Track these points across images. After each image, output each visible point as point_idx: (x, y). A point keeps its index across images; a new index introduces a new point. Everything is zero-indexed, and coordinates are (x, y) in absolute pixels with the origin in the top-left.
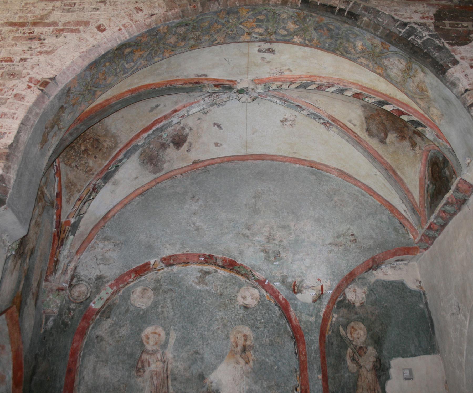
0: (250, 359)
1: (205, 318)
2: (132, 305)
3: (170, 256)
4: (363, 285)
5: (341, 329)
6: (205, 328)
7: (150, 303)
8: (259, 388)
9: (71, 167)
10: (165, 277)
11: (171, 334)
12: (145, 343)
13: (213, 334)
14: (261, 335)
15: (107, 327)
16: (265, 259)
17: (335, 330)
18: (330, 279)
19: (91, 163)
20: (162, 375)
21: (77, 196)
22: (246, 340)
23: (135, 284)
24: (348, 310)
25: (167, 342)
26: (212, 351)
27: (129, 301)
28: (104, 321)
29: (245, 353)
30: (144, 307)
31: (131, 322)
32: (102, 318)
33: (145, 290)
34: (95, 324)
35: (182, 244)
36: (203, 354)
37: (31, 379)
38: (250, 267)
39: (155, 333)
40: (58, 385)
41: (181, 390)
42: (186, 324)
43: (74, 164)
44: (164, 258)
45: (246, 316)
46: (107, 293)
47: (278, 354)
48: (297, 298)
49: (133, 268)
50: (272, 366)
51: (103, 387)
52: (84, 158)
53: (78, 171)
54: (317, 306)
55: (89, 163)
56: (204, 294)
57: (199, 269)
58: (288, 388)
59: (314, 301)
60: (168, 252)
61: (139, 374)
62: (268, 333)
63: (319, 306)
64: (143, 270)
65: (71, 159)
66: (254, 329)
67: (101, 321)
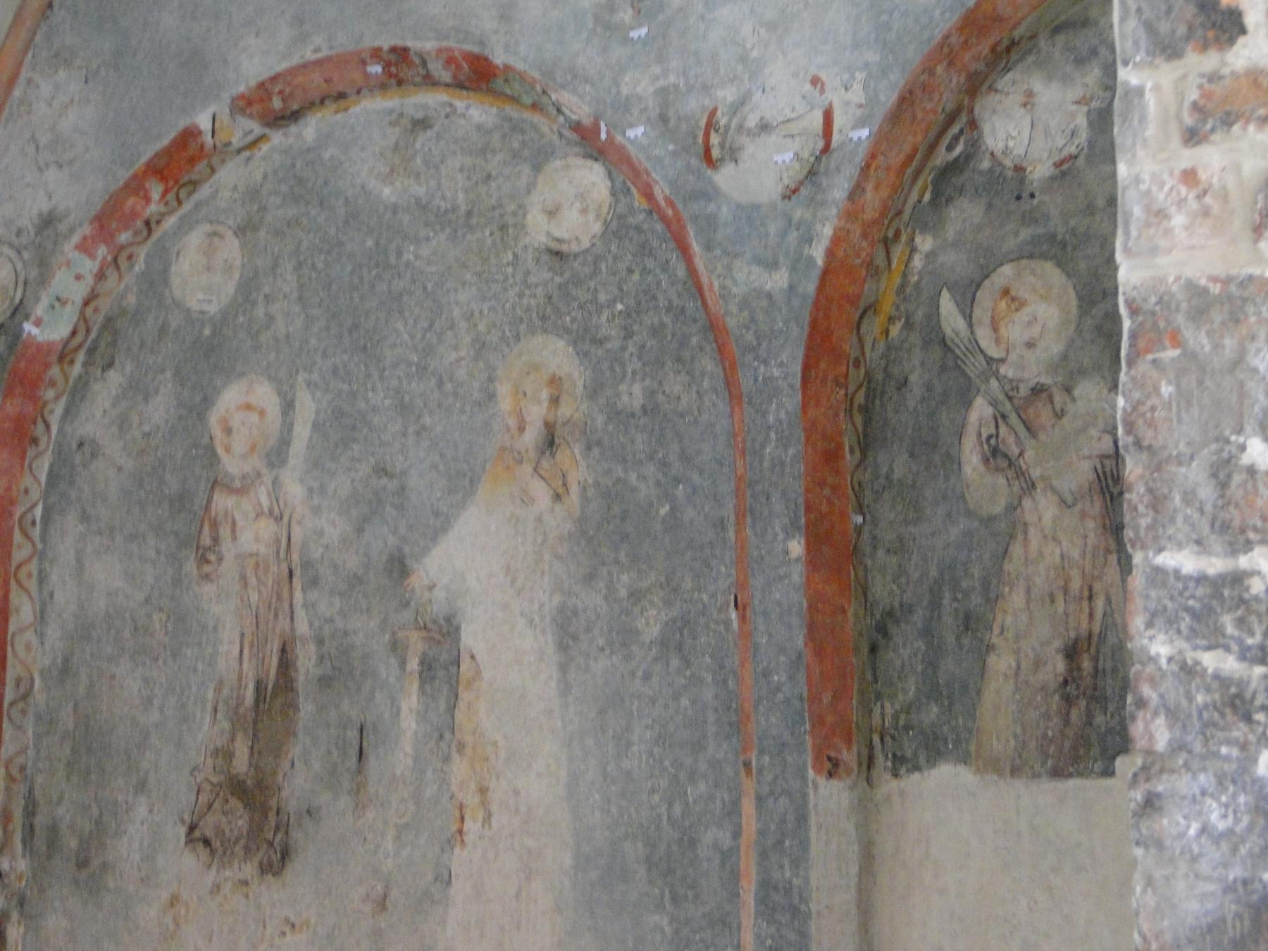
0: (570, 479)
1: (411, 322)
2: (178, 304)
3: (261, 85)
4: (1080, 62)
5: (947, 305)
6: (409, 364)
7: (230, 289)
8: (599, 600)
10: (275, 172)
11: (298, 405)
12: (220, 451)
13: (440, 384)
14: (612, 368)
15: (107, 404)
16: (597, 18)
17: (919, 315)
18: (867, 65)
20: (273, 569)
22: (555, 401)
23: (181, 219)
24: (990, 206)
25: (285, 442)
26: (437, 458)
27: (167, 292)
28: (96, 379)
29: (553, 455)
30: (213, 309)
31: (177, 373)
32: (91, 369)
33: (216, 239)
36: (404, 473)
38: (536, 75)
39: (249, 407)
41: (331, 621)
42: (345, 357)
44: (242, 96)
45: (555, 295)
47: (675, 447)
48: (717, 190)
49: (144, 160)
50: (651, 504)
51: (104, 626)
54: (798, 214)
56: (406, 218)
57: (391, 112)
58: (705, 597)
59: (791, 193)
60: (254, 63)
61: (207, 569)
62: (640, 358)
63: (808, 216)
64: (181, 163)
66: (586, 347)
67: (87, 382)
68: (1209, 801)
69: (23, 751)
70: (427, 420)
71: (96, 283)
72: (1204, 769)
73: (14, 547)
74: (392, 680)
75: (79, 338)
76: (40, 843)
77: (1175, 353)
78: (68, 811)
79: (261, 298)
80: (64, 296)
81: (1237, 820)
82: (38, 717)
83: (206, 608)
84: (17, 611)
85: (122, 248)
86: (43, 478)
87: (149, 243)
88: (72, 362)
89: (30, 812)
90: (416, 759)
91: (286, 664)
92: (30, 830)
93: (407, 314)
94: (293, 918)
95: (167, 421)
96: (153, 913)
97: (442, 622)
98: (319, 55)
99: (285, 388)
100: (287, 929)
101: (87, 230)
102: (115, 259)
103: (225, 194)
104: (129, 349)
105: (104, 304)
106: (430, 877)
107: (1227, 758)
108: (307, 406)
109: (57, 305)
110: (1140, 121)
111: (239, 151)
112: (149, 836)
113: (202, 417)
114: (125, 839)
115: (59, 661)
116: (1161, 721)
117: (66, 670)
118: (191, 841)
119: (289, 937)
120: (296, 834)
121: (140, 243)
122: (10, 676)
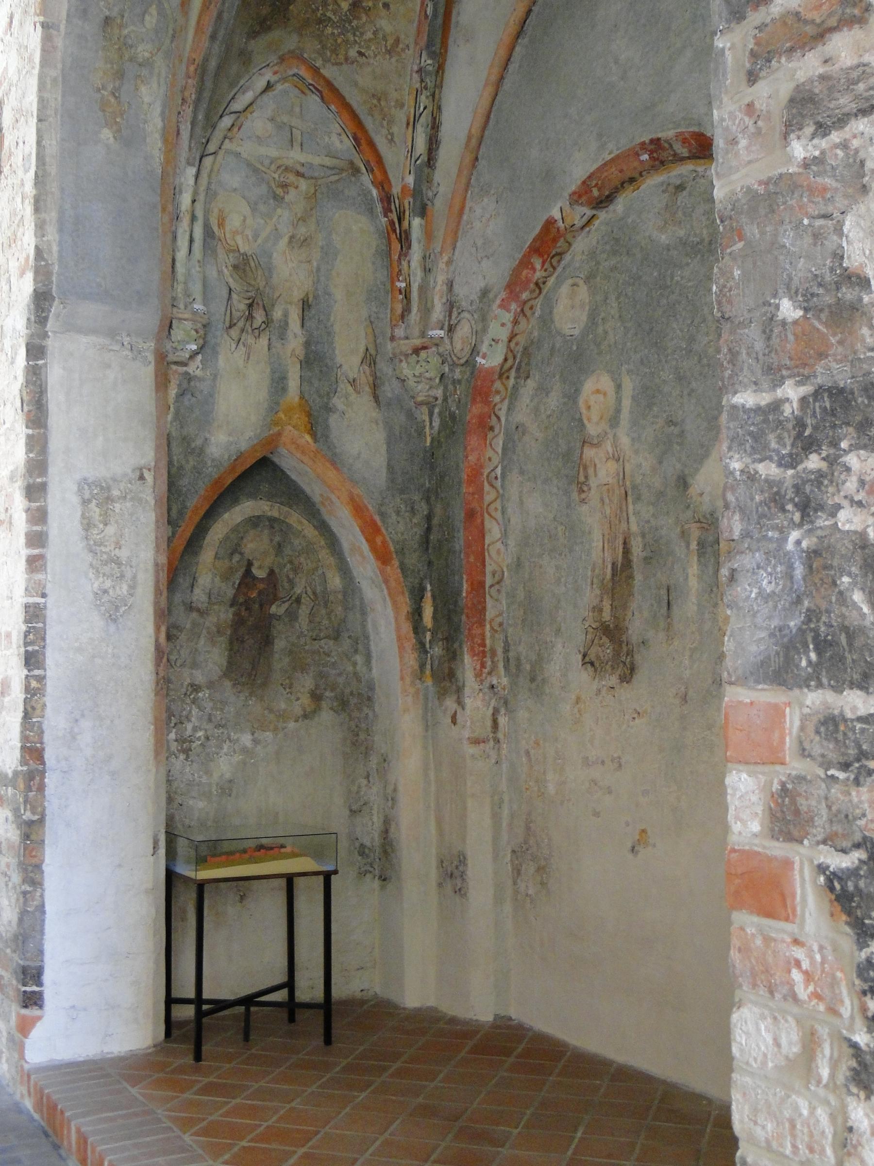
2: (559, 333)
3: (584, 182)
7: (584, 318)
9: (353, 63)
11: (623, 386)
12: (586, 422)
15: (528, 401)
19: (385, 24)
20: (617, 492)
21: (401, 116)
25: (618, 411)
30: (576, 332)
32: (519, 380)
35: (600, 136)
37: (427, 542)
39: (598, 391)
40: (457, 547)
41: (648, 522)
43: (353, 53)
44: (574, 193)
46: (503, 325)
52: (364, 24)
53: (372, 61)
55: (381, 29)
57: (662, 183)
60: (579, 168)
61: (583, 496)
64: (548, 244)
65: (339, 45)
68: (762, 572)
69: (500, 614)
70: (694, 385)
71: (513, 327)
72: (758, 550)
74: (683, 556)
75: (510, 362)
77: (740, 245)
79: (600, 320)
80: (496, 338)
81: (777, 584)
82: (507, 594)
84: (490, 531)
85: (525, 303)
86: (500, 451)
87: (542, 296)
88: (508, 377)
89: (506, 650)
90: (699, 605)
91: (627, 551)
92: (507, 660)
93: (678, 316)
94: (638, 709)
96: (568, 707)
97: (708, 516)
98: (612, 156)
99: (617, 376)
100: (636, 716)
101: (503, 295)
102: (522, 310)
103: (578, 258)
104: (537, 365)
106: (710, 681)
107: (770, 540)
108: (628, 385)
109: (493, 343)
110: (723, 75)
111: (583, 228)
112: (563, 659)
113: (575, 402)
114: (552, 663)
116: (737, 517)
117: (518, 564)
119: (637, 721)
120: (637, 657)
121: (535, 298)
122: (489, 569)
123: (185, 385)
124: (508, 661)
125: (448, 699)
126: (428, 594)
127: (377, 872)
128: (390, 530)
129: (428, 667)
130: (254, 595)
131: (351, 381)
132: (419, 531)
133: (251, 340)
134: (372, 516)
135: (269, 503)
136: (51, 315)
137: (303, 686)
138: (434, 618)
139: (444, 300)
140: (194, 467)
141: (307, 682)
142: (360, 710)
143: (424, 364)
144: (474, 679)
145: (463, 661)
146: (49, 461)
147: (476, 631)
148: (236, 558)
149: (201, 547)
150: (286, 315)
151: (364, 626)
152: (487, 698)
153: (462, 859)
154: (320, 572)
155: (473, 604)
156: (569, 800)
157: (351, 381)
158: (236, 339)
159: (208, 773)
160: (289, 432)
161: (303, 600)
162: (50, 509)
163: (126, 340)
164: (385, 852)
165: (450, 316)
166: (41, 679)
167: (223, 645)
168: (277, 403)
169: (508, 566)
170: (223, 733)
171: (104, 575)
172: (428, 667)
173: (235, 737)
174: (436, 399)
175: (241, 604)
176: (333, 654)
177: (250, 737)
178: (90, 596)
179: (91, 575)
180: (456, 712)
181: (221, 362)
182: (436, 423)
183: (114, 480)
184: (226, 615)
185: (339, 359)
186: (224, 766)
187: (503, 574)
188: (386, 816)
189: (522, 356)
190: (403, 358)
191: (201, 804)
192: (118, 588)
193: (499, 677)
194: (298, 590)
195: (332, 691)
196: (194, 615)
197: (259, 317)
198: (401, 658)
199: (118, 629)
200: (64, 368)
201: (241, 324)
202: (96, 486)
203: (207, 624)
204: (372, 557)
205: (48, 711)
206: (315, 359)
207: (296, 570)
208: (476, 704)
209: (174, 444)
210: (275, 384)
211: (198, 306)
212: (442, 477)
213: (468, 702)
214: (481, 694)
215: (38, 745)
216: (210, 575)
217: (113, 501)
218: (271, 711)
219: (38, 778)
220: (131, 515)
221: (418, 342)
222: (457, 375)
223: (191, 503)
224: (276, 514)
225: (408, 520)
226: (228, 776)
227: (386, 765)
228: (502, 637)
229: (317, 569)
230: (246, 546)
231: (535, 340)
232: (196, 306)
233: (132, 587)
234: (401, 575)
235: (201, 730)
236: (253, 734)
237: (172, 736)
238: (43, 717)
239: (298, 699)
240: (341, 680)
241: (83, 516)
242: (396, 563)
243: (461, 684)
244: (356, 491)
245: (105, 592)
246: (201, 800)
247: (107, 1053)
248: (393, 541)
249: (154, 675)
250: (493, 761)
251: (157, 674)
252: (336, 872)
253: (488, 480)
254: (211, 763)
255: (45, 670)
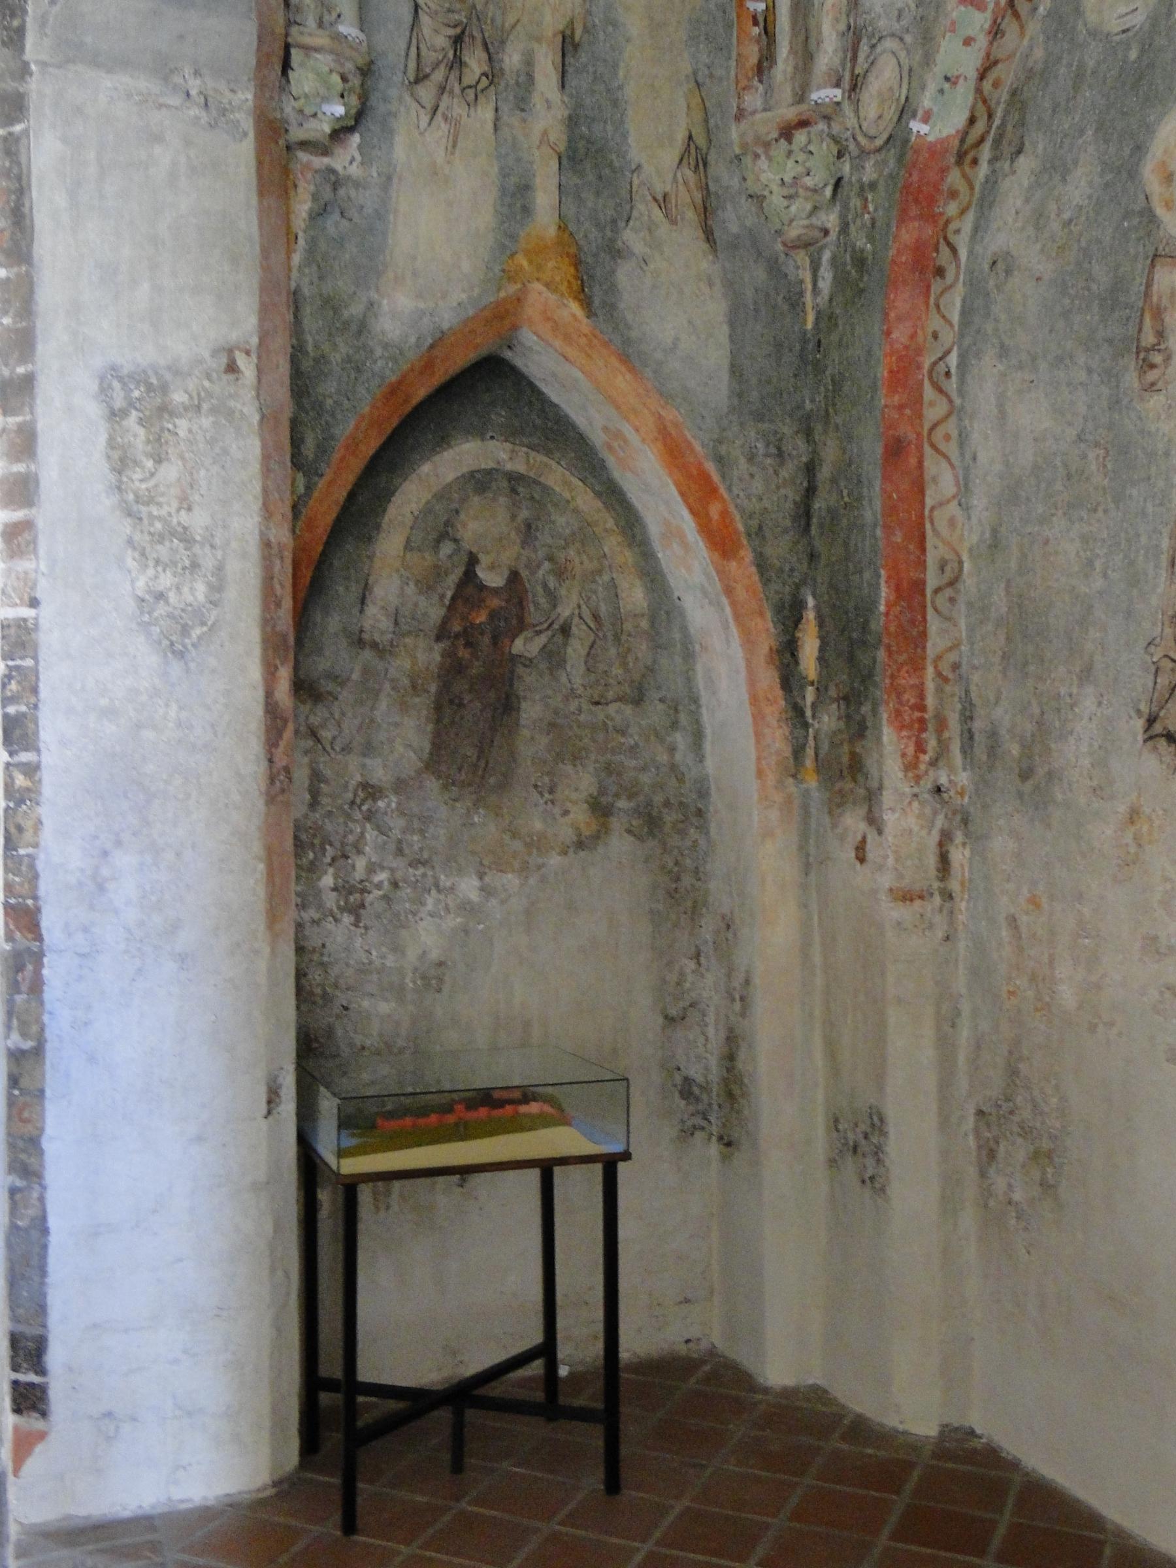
12: (1160, 211)
15: (1019, 203)
32: (998, 165)
34: (982, 207)
37: (808, 514)
40: (868, 516)
46: (968, 41)
61: (1152, 376)
69: (955, 646)
71: (991, 43)
73: (925, 405)
75: (980, 126)
76: (980, 752)
78: (1006, 713)
82: (970, 605)
83: (1153, 429)
84: (935, 479)
86: (955, 318)
88: (975, 162)
89: (967, 717)
95: (1090, 197)
105: (1007, 74)
109: (947, 86)
115: (987, 535)
117: (995, 544)
118: (1151, 738)
123: (327, 193)
124: (971, 738)
125: (848, 814)
126: (810, 615)
127: (714, 1130)
128: (735, 491)
129: (810, 752)
130: (481, 618)
131: (660, 198)
132: (792, 494)
133: (459, 110)
134: (700, 464)
135: (508, 445)
136: (29, 20)
137: (576, 790)
138: (821, 659)
139: (842, 27)
140: (348, 359)
141: (582, 781)
142: (682, 833)
143: (801, 157)
144: (900, 775)
145: (879, 740)
146: (38, 332)
147: (906, 680)
148: (447, 548)
149: (378, 527)
150: (529, 62)
151: (689, 680)
152: (928, 811)
153: (876, 1123)
154: (606, 577)
155: (900, 626)
156: (1111, 1024)
157: (660, 198)
158: (429, 106)
159: (397, 949)
160: (539, 296)
161: (574, 630)
162: (40, 426)
163: (194, 85)
164: (730, 1095)
165: (855, 58)
166: (31, 770)
167: (425, 712)
168: (513, 237)
169: (970, 550)
170: (424, 875)
171: (157, 562)
172: (810, 752)
173: (448, 884)
174: (826, 232)
175: (457, 636)
176: (633, 730)
177: (476, 882)
178: (131, 605)
179: (130, 563)
180: (864, 840)
181: (400, 151)
182: (825, 285)
183: (177, 372)
184: (427, 655)
185: (635, 154)
186: (428, 936)
187: (961, 569)
188: (731, 1030)
189: (1007, 113)
190: (760, 151)
191: (384, 1007)
192: (186, 590)
193: (952, 769)
194: (564, 611)
195: (630, 797)
196: (367, 654)
197: (475, 63)
198: (758, 735)
199: (188, 671)
200: (65, 140)
201: (438, 76)
202: (138, 383)
203: (393, 673)
204: (701, 544)
205: (47, 836)
206: (587, 154)
207: (561, 573)
208: (906, 823)
209: (307, 310)
210: (508, 200)
211: (348, 29)
212: (837, 384)
213: (890, 819)
214: (915, 804)
215: (30, 902)
216: (396, 582)
217: (173, 414)
218: (515, 835)
219: (30, 967)
220: (211, 442)
221: (790, 113)
222: (869, 172)
223: (345, 429)
224: (520, 467)
225: (771, 471)
226: (434, 955)
227: (730, 935)
228: (958, 690)
229: (600, 572)
230: (464, 525)
231: (1040, 66)
232: (343, 29)
233: (217, 588)
234: (756, 578)
235: (383, 868)
236: (481, 878)
237: (328, 880)
238: (36, 845)
239: (566, 813)
240: (646, 779)
241: (111, 444)
242: (747, 555)
243: (874, 784)
244: (670, 414)
245: (160, 596)
246: (386, 1000)
247: (182, 1501)
248: (742, 511)
249: (264, 764)
250: (940, 934)
251: (270, 761)
252: (626, 1156)
253: (931, 378)
254: (404, 932)
255: (38, 751)
